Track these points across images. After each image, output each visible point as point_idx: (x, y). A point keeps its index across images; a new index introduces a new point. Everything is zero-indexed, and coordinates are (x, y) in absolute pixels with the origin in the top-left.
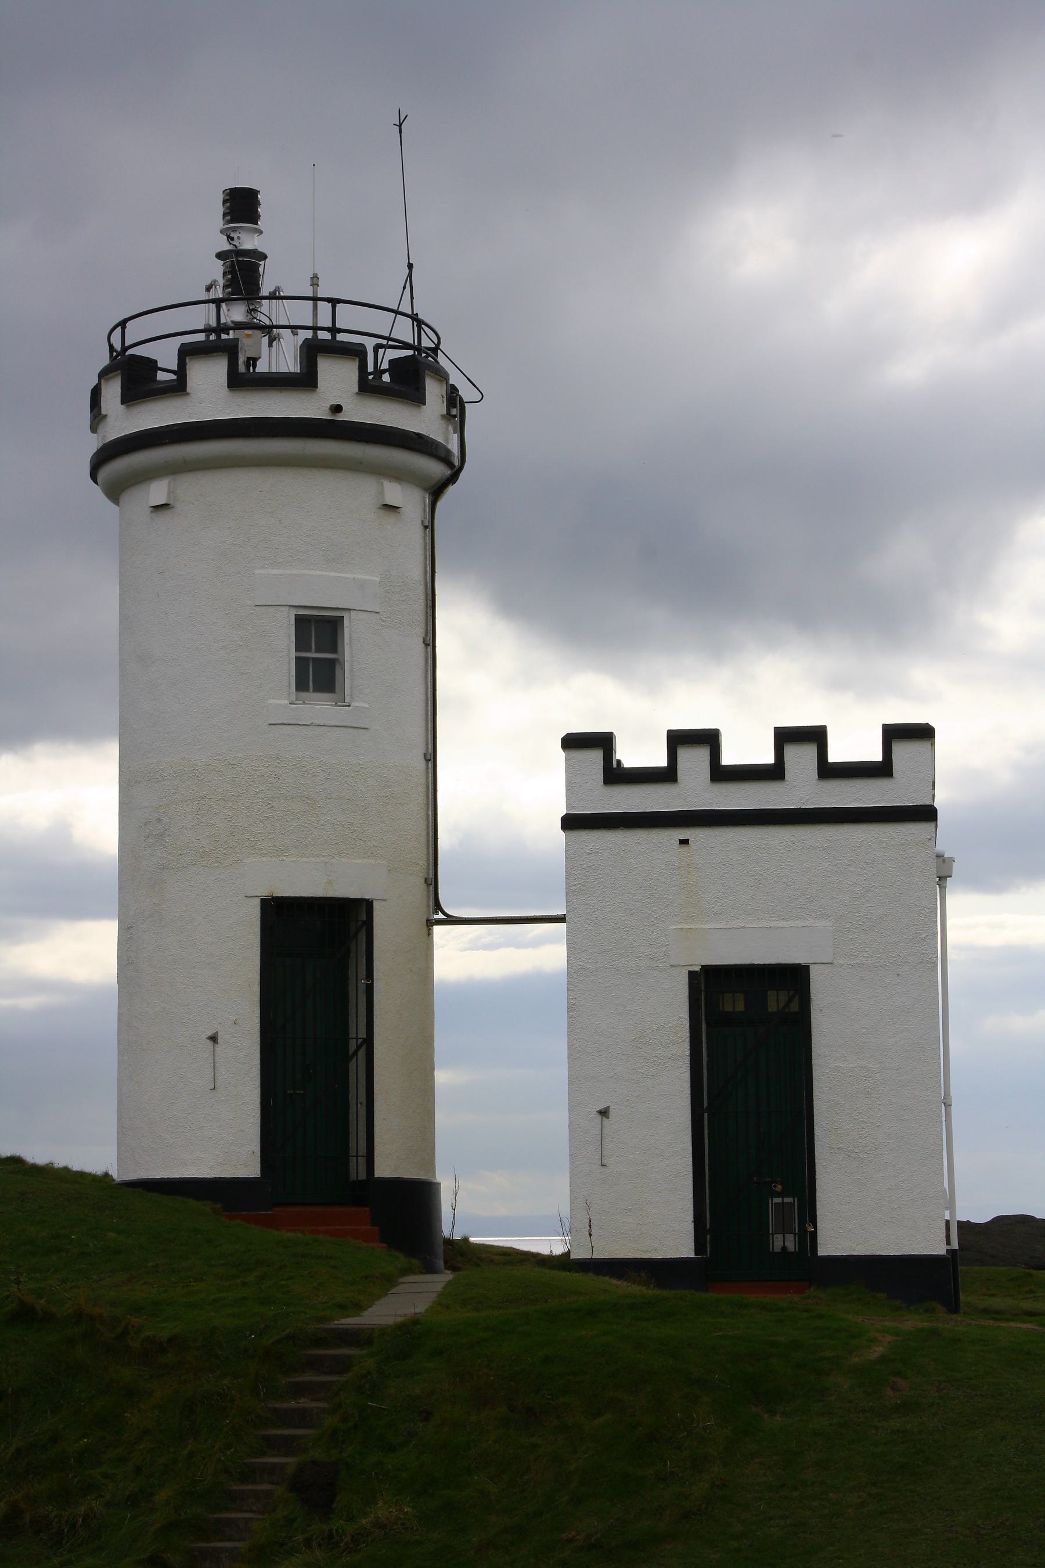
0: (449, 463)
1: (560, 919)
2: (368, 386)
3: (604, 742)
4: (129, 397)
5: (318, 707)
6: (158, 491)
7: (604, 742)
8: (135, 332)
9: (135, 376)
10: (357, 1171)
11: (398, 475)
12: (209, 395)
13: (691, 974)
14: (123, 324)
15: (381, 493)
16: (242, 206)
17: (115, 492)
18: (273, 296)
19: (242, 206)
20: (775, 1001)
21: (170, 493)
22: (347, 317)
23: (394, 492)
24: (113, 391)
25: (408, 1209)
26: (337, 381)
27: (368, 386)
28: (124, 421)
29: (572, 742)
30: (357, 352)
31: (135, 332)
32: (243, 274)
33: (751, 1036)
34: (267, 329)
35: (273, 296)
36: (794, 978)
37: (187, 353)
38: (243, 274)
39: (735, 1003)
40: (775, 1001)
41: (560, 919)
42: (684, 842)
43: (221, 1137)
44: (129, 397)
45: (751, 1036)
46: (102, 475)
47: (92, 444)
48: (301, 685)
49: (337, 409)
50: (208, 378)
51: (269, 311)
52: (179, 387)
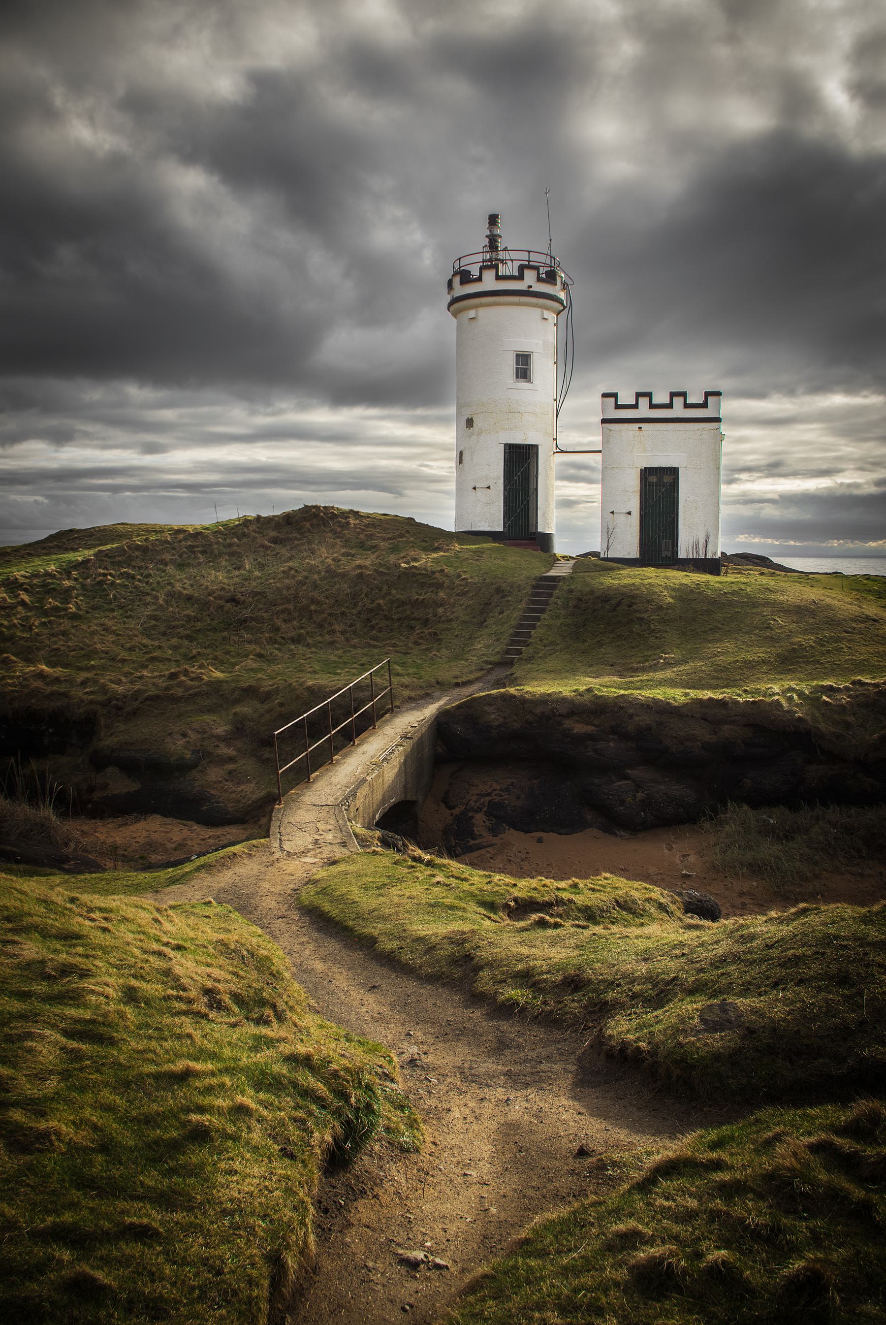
0: (563, 304)
1: (600, 452)
2: (539, 280)
3: (615, 395)
4: (462, 283)
5: (523, 384)
6: (472, 313)
7: (615, 395)
8: (464, 262)
9: (465, 277)
10: (532, 530)
11: (548, 308)
12: (489, 282)
13: (641, 470)
14: (459, 259)
15: (543, 314)
16: (493, 220)
17: (455, 314)
18: (505, 249)
19: (493, 220)
20: (667, 479)
21: (476, 314)
22: (533, 257)
23: (547, 314)
24: (457, 280)
25: (544, 542)
26: (530, 277)
27: (539, 280)
28: (460, 290)
29: (605, 395)
30: (537, 268)
31: (464, 262)
32: (493, 243)
33: (659, 491)
34: (502, 261)
35: (505, 249)
36: (674, 472)
37: (482, 269)
38: (493, 243)
39: (653, 479)
40: (667, 479)
41: (600, 452)
42: (640, 428)
43: (491, 515)
44: (462, 283)
45: (659, 491)
46: (451, 309)
47: (448, 298)
48: (517, 377)
49: (531, 287)
50: (489, 276)
51: (502, 255)
52: (479, 279)
